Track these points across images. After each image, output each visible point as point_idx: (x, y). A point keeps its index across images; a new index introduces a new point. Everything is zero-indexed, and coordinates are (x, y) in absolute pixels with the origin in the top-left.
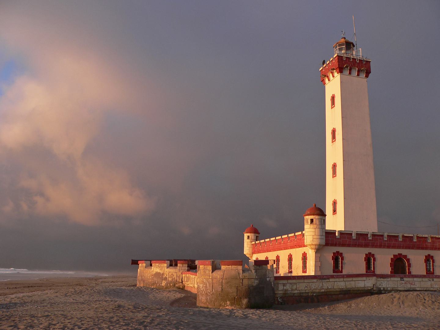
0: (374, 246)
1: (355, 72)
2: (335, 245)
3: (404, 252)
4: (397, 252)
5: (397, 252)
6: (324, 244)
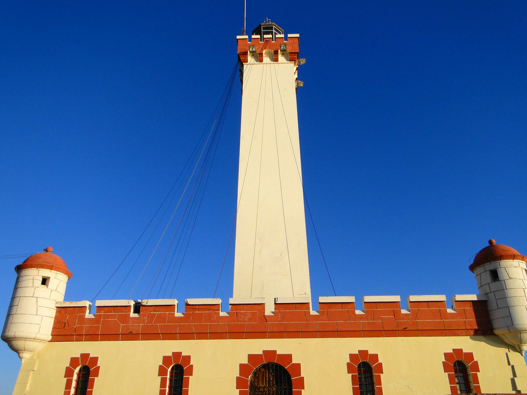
0: (92, 337)
2: (80, 337)
3: (281, 346)
4: (259, 346)
5: (259, 346)
6: (50, 338)
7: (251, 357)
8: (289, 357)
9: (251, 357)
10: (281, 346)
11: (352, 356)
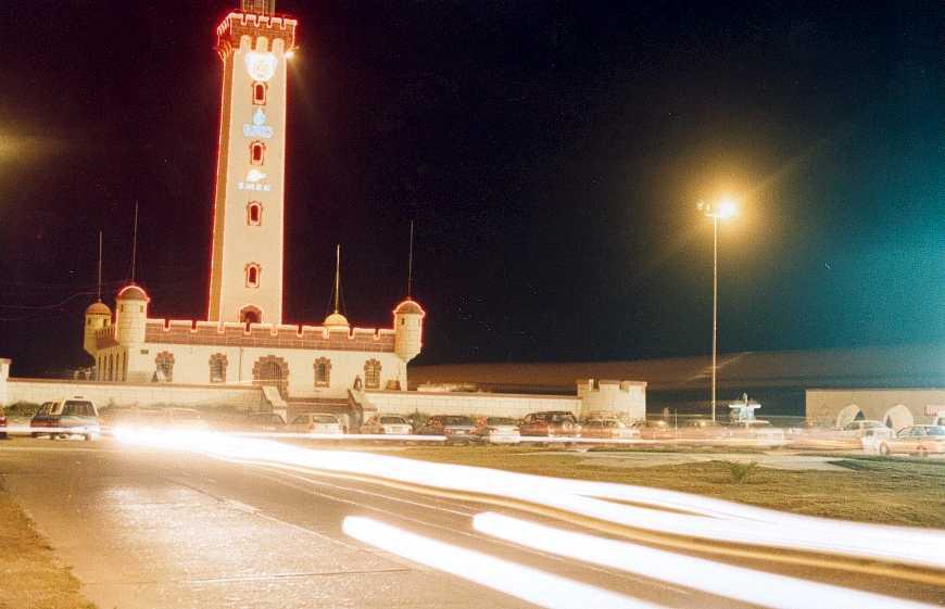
1: (262, 41)
3: (277, 353)
4: (265, 352)
5: (265, 352)
7: (261, 359)
8: (281, 359)
9: (261, 359)
10: (277, 353)
11: (213, 356)
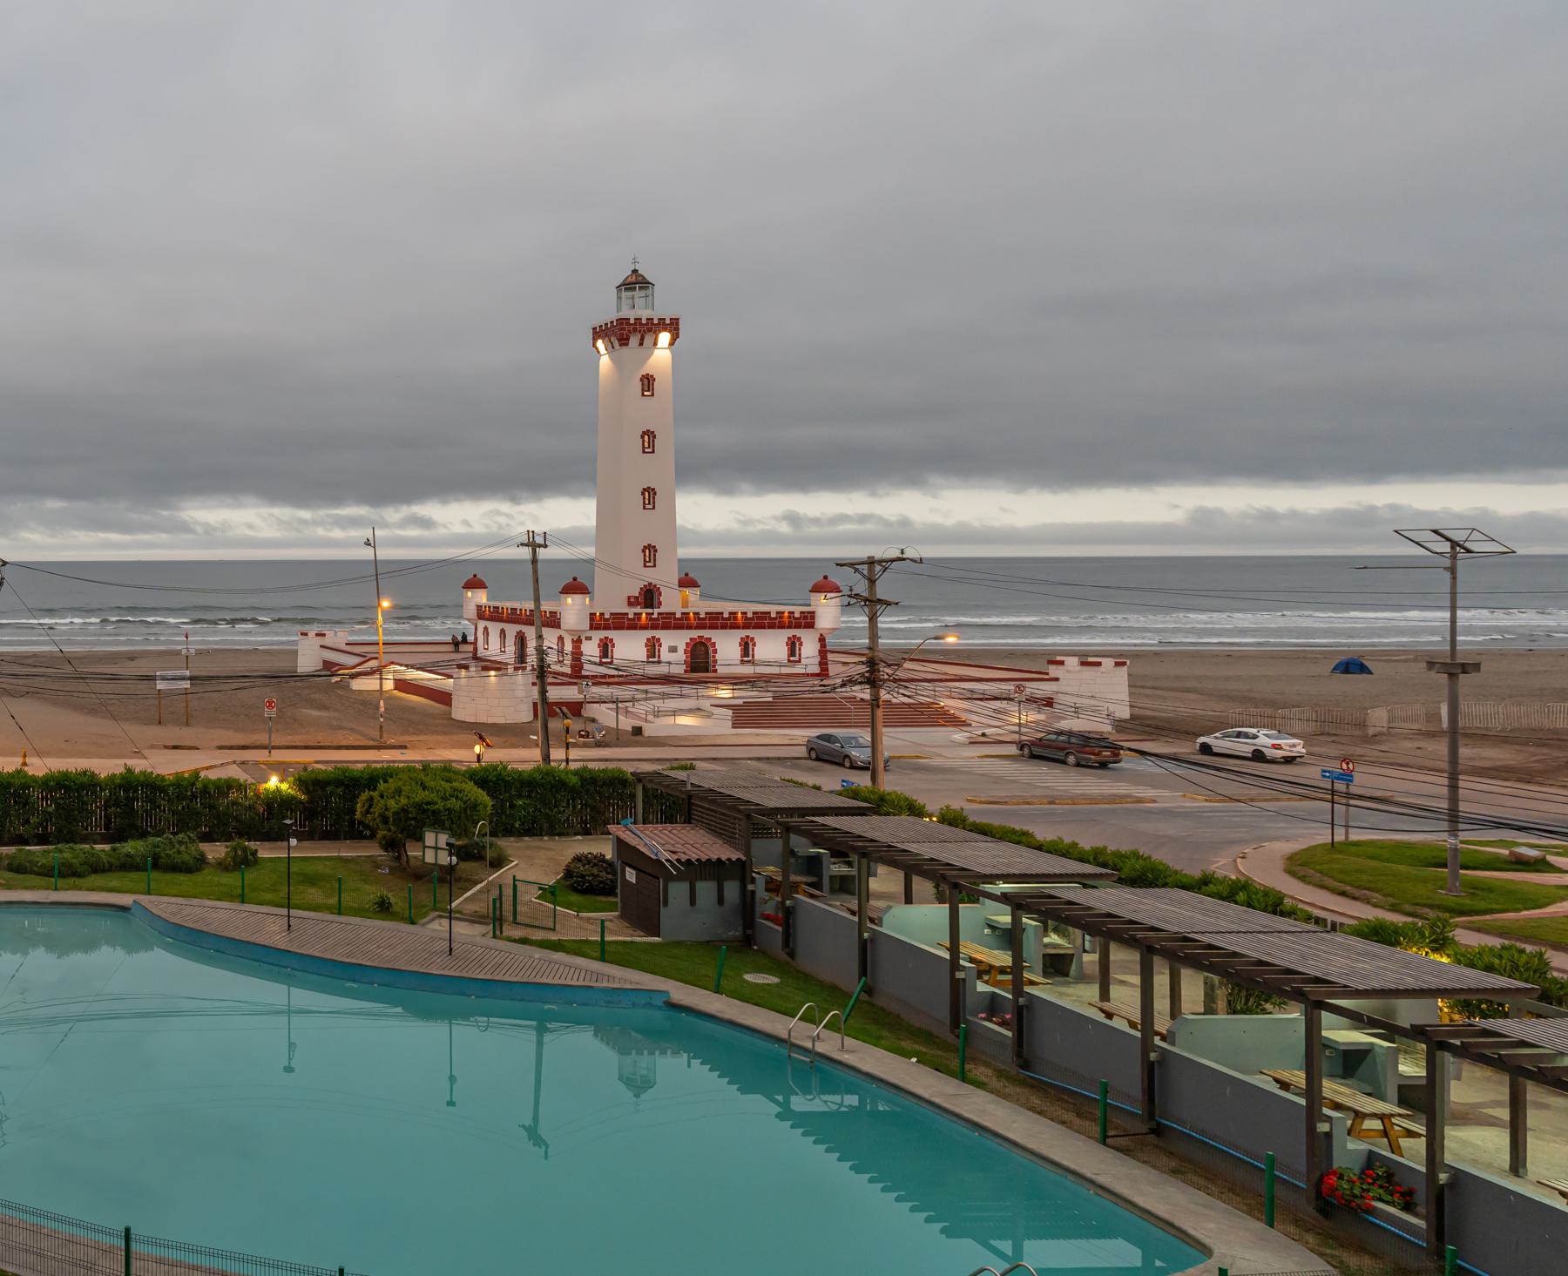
4: (695, 634)
10: (706, 633)
